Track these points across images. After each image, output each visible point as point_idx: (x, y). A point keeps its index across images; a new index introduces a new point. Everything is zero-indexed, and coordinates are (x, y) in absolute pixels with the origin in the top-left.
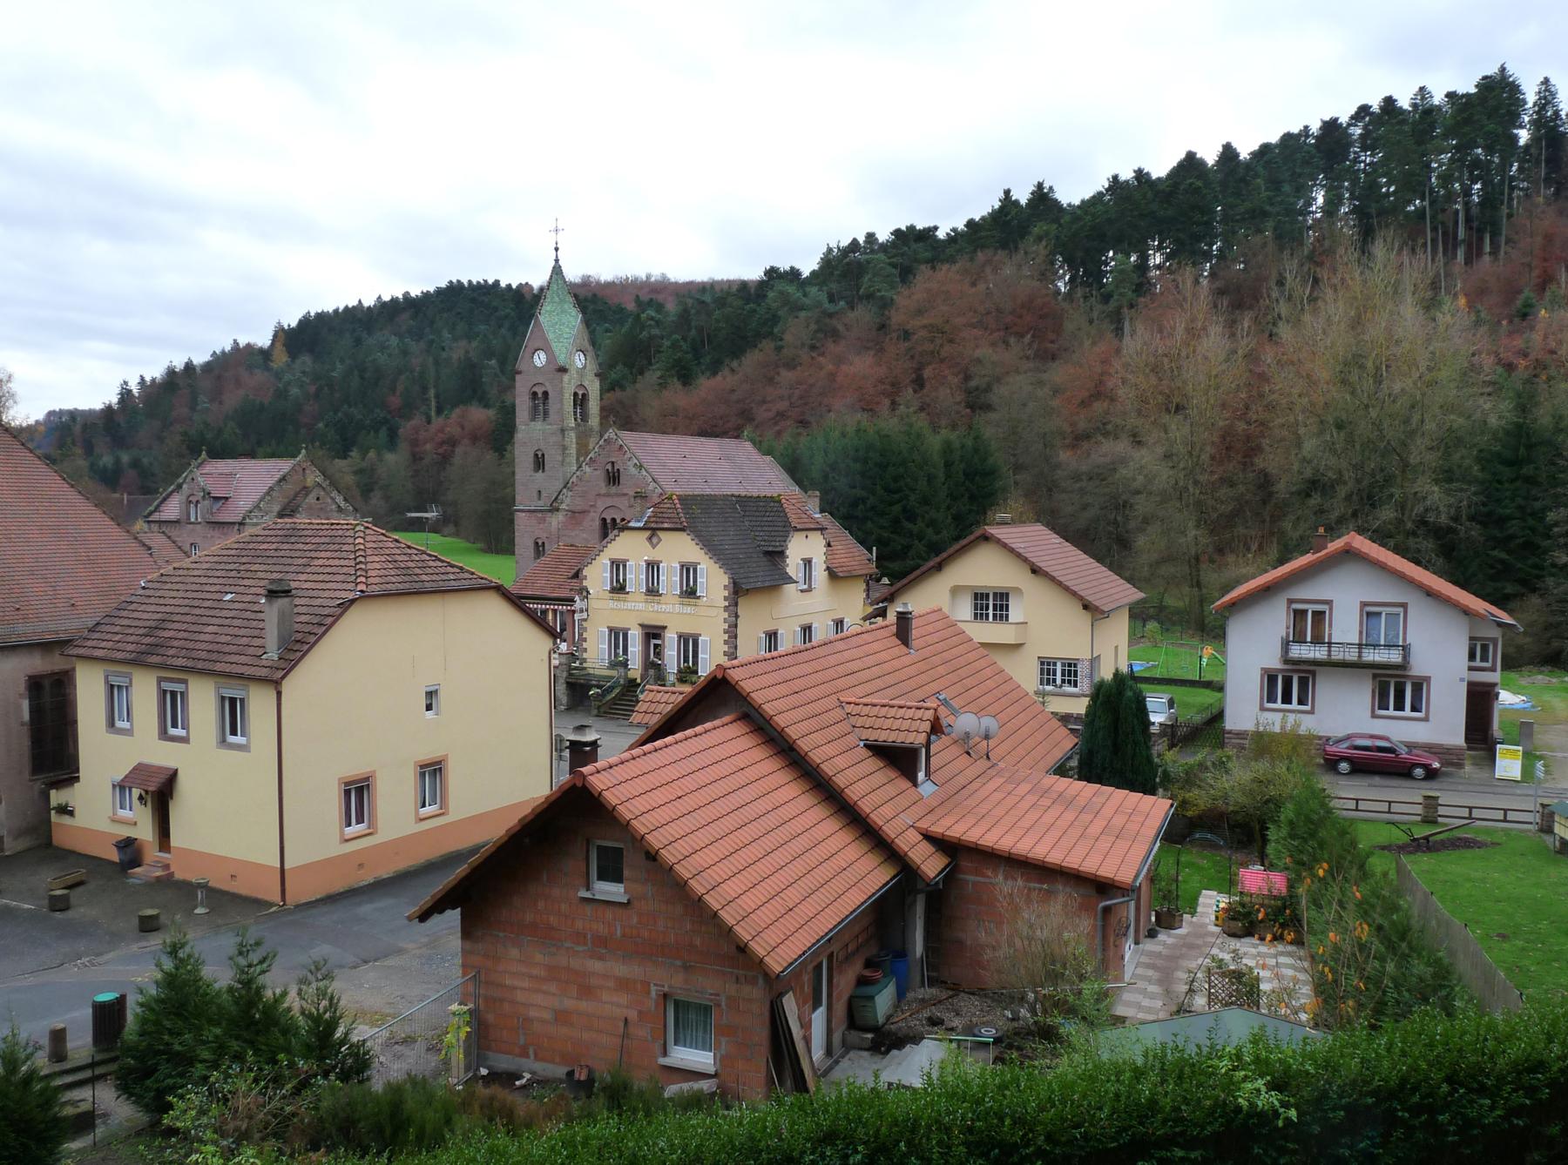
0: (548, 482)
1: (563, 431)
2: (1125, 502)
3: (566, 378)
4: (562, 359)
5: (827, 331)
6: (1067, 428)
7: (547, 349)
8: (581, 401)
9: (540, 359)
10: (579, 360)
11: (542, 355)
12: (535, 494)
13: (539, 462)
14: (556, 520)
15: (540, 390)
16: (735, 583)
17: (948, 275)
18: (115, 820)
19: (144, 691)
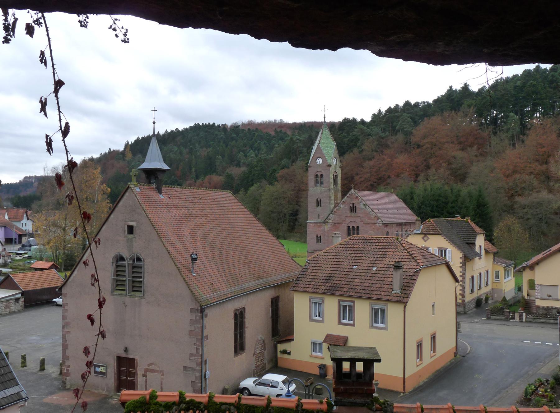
0: (323, 211)
1: (330, 190)
3: (331, 169)
4: (329, 162)
5: (382, 146)
6: (402, 175)
7: (323, 158)
8: (335, 178)
9: (319, 161)
10: (334, 162)
11: (321, 160)
12: (317, 216)
13: (319, 203)
14: (327, 227)
15: (319, 174)
16: (465, 256)
17: (436, 120)
18: (312, 356)
19: (331, 305)
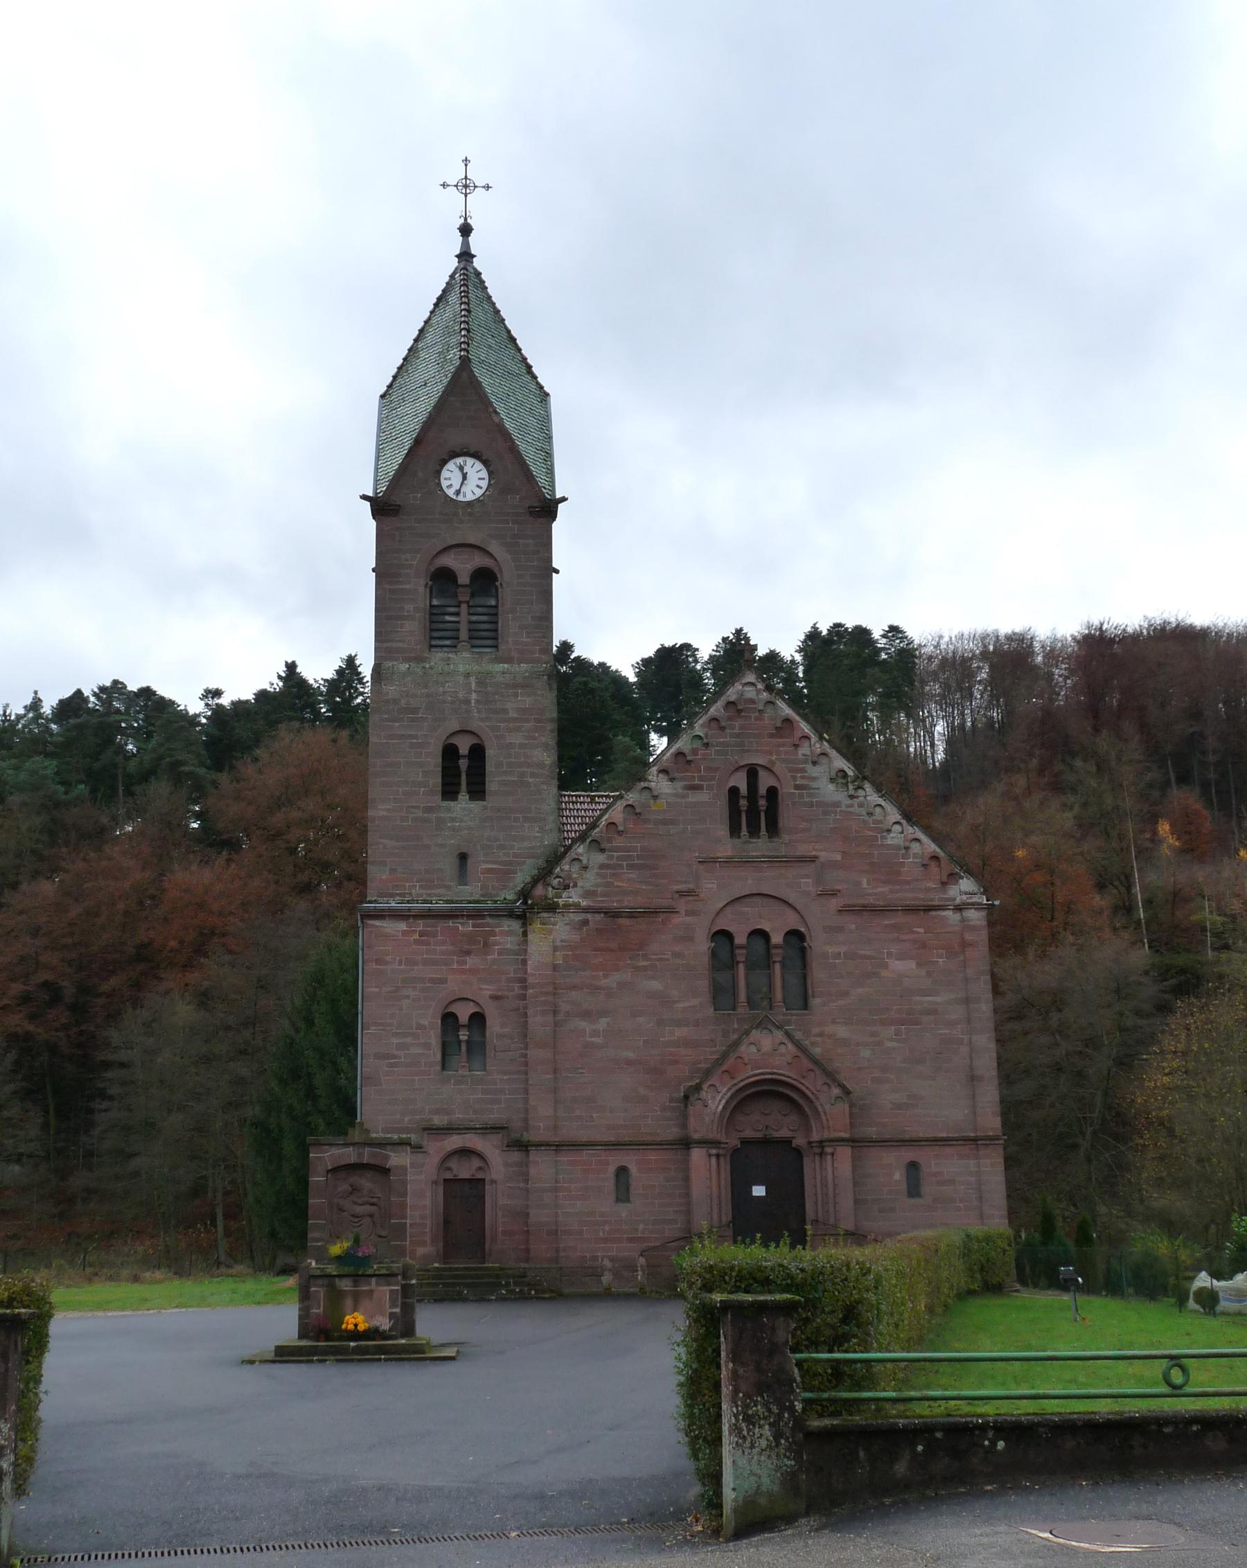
2: (1101, 886)
11: (450, 477)
12: (448, 865)
14: (548, 940)
